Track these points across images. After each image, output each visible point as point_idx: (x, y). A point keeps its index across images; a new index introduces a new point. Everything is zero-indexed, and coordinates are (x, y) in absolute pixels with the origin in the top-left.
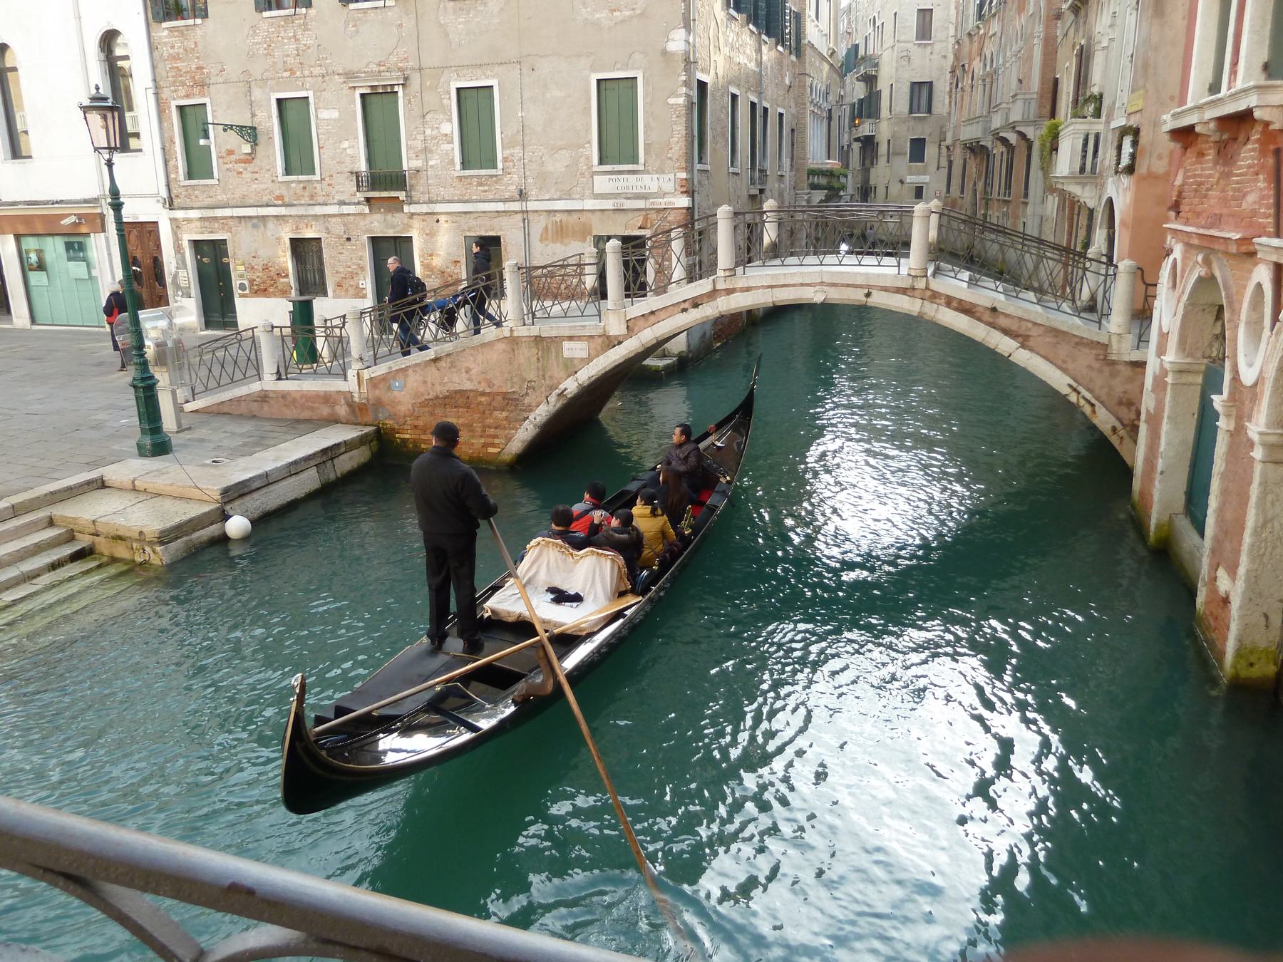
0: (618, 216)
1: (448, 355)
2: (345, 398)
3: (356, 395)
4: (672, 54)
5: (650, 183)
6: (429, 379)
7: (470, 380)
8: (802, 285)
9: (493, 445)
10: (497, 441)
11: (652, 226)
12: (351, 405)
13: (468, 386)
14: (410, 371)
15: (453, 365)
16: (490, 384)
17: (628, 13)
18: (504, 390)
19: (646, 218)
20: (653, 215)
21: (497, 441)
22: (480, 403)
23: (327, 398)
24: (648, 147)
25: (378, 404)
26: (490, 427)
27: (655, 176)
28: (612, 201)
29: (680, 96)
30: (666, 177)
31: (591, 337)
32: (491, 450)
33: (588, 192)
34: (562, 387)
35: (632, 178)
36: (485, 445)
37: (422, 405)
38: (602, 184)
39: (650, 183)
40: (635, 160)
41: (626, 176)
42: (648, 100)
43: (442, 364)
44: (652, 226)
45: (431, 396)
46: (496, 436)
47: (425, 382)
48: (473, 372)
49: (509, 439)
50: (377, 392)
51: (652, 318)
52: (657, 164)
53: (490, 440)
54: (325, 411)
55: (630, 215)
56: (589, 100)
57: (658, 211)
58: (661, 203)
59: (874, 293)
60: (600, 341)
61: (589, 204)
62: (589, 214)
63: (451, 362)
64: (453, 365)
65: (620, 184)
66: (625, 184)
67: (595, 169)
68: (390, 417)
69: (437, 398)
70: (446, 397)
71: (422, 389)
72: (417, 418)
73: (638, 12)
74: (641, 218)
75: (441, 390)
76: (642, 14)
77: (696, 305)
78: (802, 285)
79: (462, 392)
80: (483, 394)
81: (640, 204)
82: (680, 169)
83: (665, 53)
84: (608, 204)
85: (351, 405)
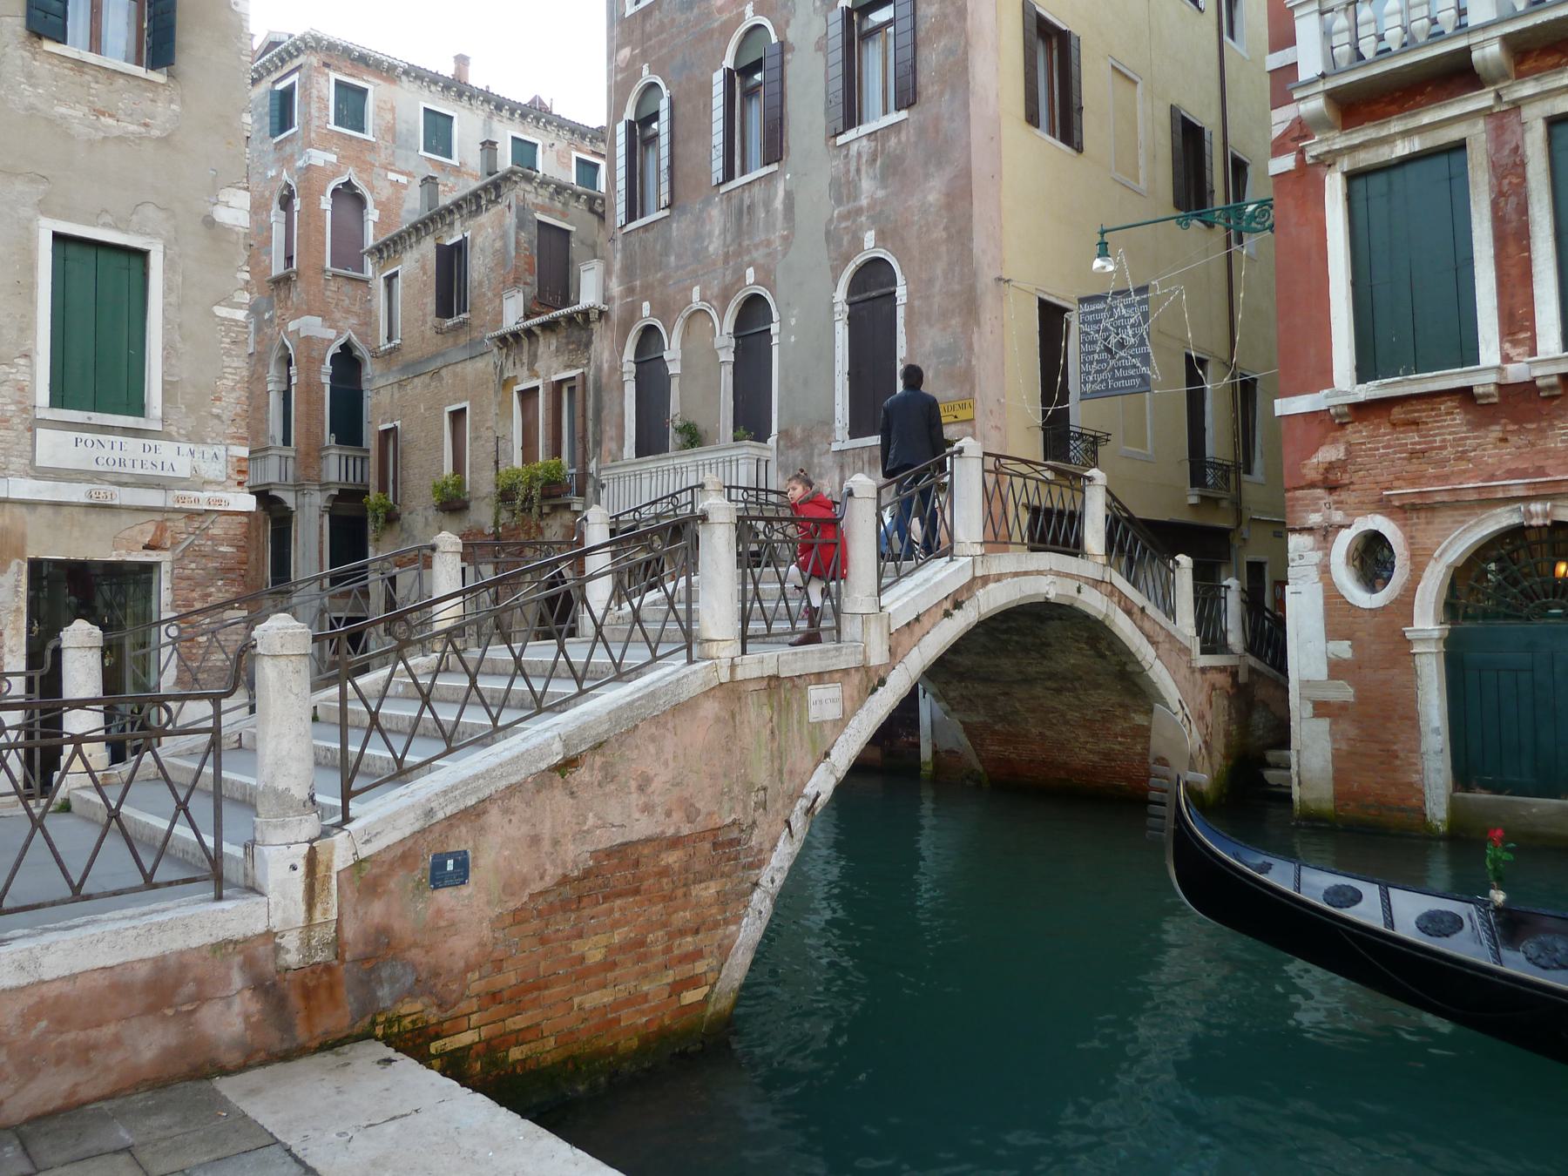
0: (94, 518)
1: (598, 746)
2: (249, 964)
3: (291, 942)
4: (227, 230)
5: (174, 458)
6: (546, 830)
7: (647, 809)
8: (1016, 574)
9: (693, 982)
10: (700, 967)
11: (175, 544)
12: (268, 987)
13: (642, 827)
14: (494, 816)
15: (609, 775)
16: (691, 815)
17: (132, 128)
18: (717, 821)
19: (161, 528)
20: (180, 523)
21: (700, 967)
22: (665, 872)
23: (165, 988)
24: (169, 388)
25: (381, 948)
26: (682, 933)
27: (185, 447)
28: (86, 487)
29: (239, 306)
30: (209, 451)
31: (846, 671)
32: (690, 997)
33: (18, 463)
34: (810, 790)
35: (132, 444)
36: (679, 987)
37: (518, 917)
38: (55, 447)
39: (174, 458)
40: (139, 409)
41: (117, 439)
42: (173, 299)
43: (582, 775)
44: (175, 544)
45: (549, 881)
46: (697, 955)
47: (535, 840)
48: (656, 785)
49: (725, 951)
50: (377, 910)
51: (917, 628)
52: (190, 423)
53: (685, 970)
54: (149, 1043)
55: (126, 519)
56: (31, 268)
57: (192, 514)
58: (202, 499)
59: (1085, 588)
60: (856, 678)
61: (24, 488)
62: (20, 511)
63: (605, 767)
64: (609, 775)
65: (105, 453)
66: (116, 454)
67: (40, 414)
68: (420, 987)
69: (565, 880)
70: (587, 874)
71: (524, 867)
72: (498, 965)
73: (156, 133)
74: (151, 528)
75: (576, 855)
76: (165, 141)
77: (958, 605)
78: (1016, 574)
79: (620, 852)
80: (675, 842)
81: (153, 498)
82: (241, 440)
83: (210, 222)
84: (76, 493)
85: (270, 989)
